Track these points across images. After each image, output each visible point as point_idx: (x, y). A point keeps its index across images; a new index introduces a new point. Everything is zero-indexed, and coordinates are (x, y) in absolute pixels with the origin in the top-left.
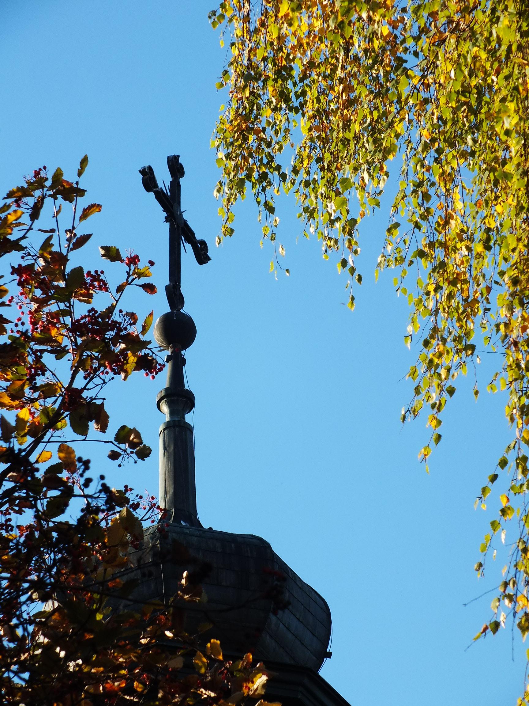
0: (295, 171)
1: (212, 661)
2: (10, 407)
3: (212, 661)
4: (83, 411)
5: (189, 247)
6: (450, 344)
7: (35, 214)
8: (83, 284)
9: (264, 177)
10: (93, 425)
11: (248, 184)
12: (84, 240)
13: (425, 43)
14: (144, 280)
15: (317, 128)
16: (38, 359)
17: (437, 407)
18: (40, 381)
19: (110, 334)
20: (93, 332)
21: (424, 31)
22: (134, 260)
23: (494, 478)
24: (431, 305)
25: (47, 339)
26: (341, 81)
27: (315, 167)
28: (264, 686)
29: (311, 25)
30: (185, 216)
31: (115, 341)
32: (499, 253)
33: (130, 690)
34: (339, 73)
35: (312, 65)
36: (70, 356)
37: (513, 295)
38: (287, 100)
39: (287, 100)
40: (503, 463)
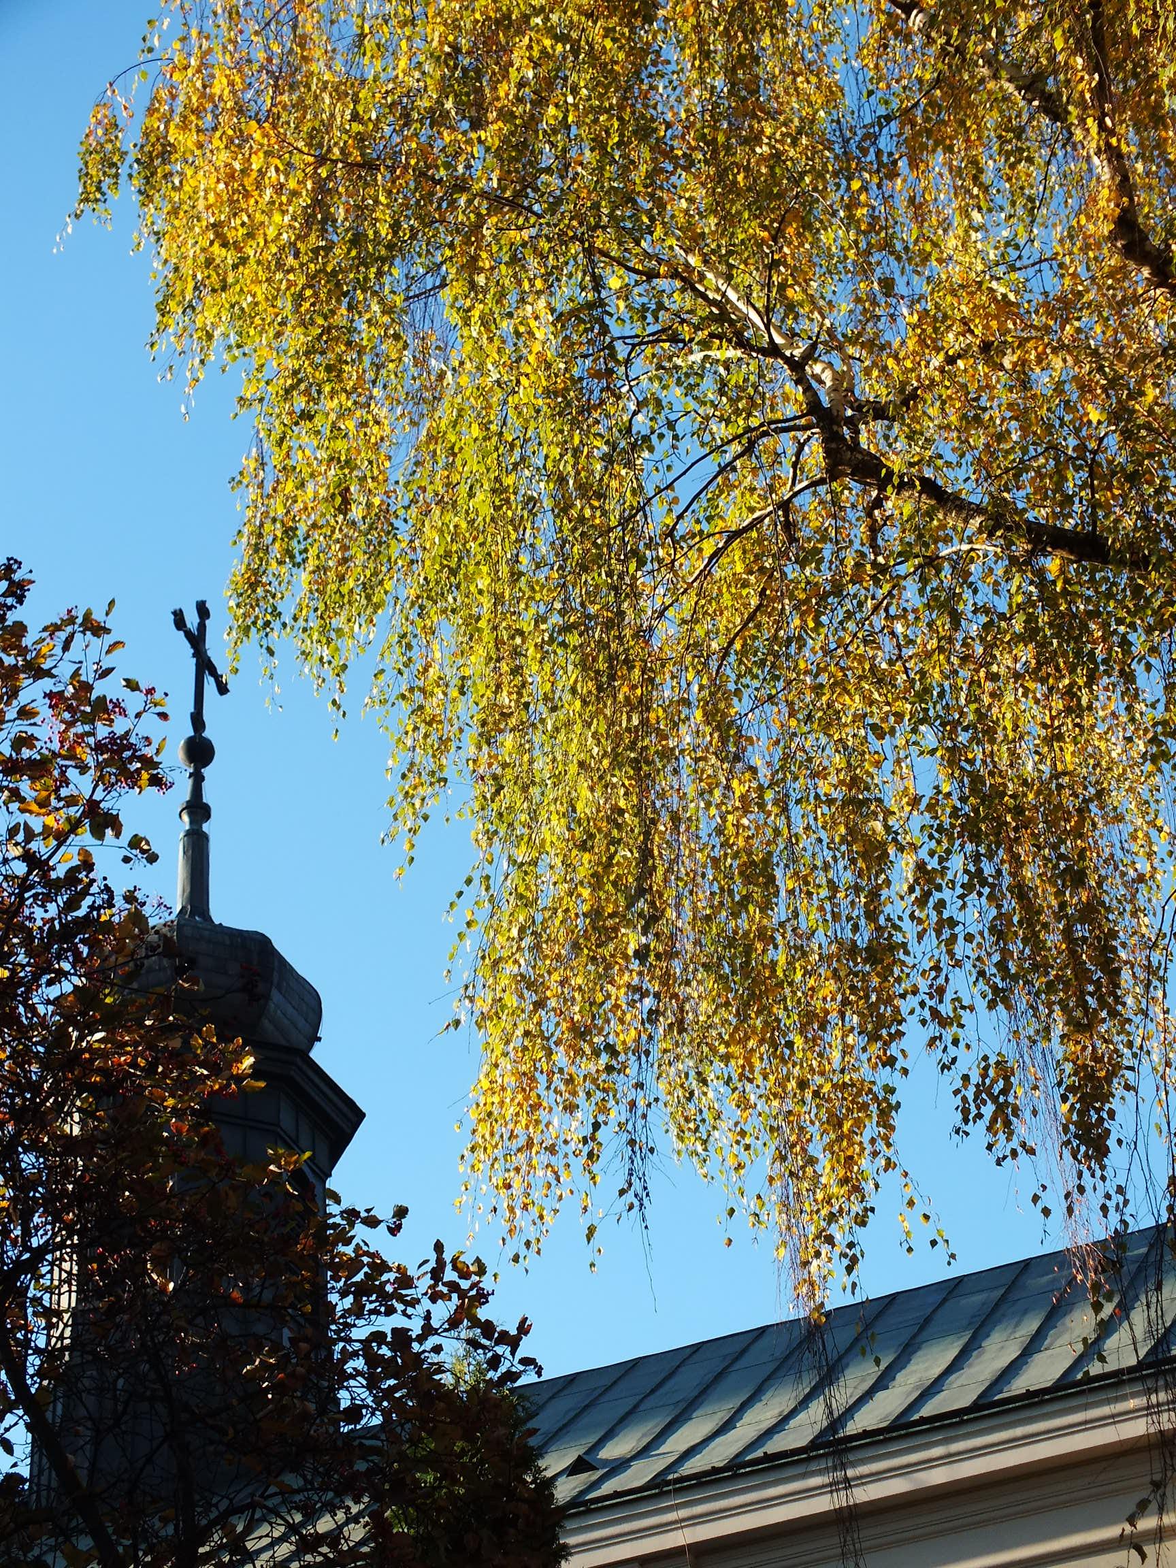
0: (295, 619)
1: (207, 1043)
2: (38, 814)
3: (207, 1043)
4: (100, 820)
5: (212, 680)
6: (424, 777)
7: (66, 648)
8: (106, 711)
9: (267, 624)
10: (109, 832)
11: (253, 629)
12: (107, 672)
13: (414, 511)
14: (159, 709)
15: (316, 582)
16: (63, 773)
17: (413, 831)
18: (64, 792)
19: (127, 754)
20: (112, 751)
21: (414, 501)
22: (150, 691)
23: (460, 894)
24: (409, 743)
25: (71, 756)
26: (338, 541)
27: (312, 615)
28: (251, 1066)
29: (316, 493)
30: (209, 653)
31: (131, 760)
32: (471, 698)
33: (134, 1065)
34: (337, 535)
35: (314, 526)
36: (92, 771)
37: (481, 735)
38: (292, 557)
39: (292, 557)
40: (469, 881)
